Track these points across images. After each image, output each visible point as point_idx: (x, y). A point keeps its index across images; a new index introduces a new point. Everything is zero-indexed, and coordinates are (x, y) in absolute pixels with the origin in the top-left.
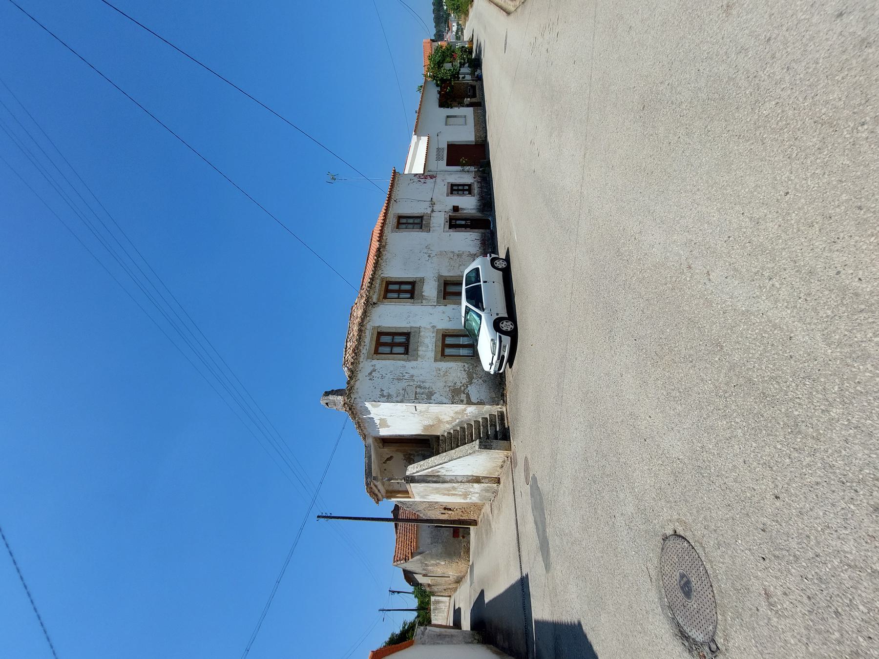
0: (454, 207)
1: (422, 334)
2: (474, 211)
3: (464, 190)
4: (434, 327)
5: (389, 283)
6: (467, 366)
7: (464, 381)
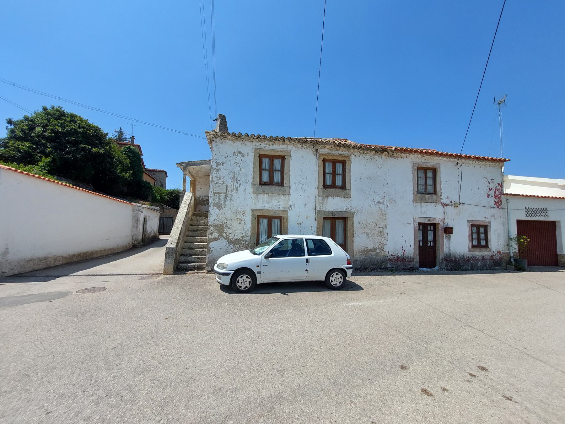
0: (451, 228)
1: (282, 197)
2: (446, 250)
3: (479, 239)
4: (290, 208)
5: (343, 163)
6: (248, 239)
7: (231, 236)
